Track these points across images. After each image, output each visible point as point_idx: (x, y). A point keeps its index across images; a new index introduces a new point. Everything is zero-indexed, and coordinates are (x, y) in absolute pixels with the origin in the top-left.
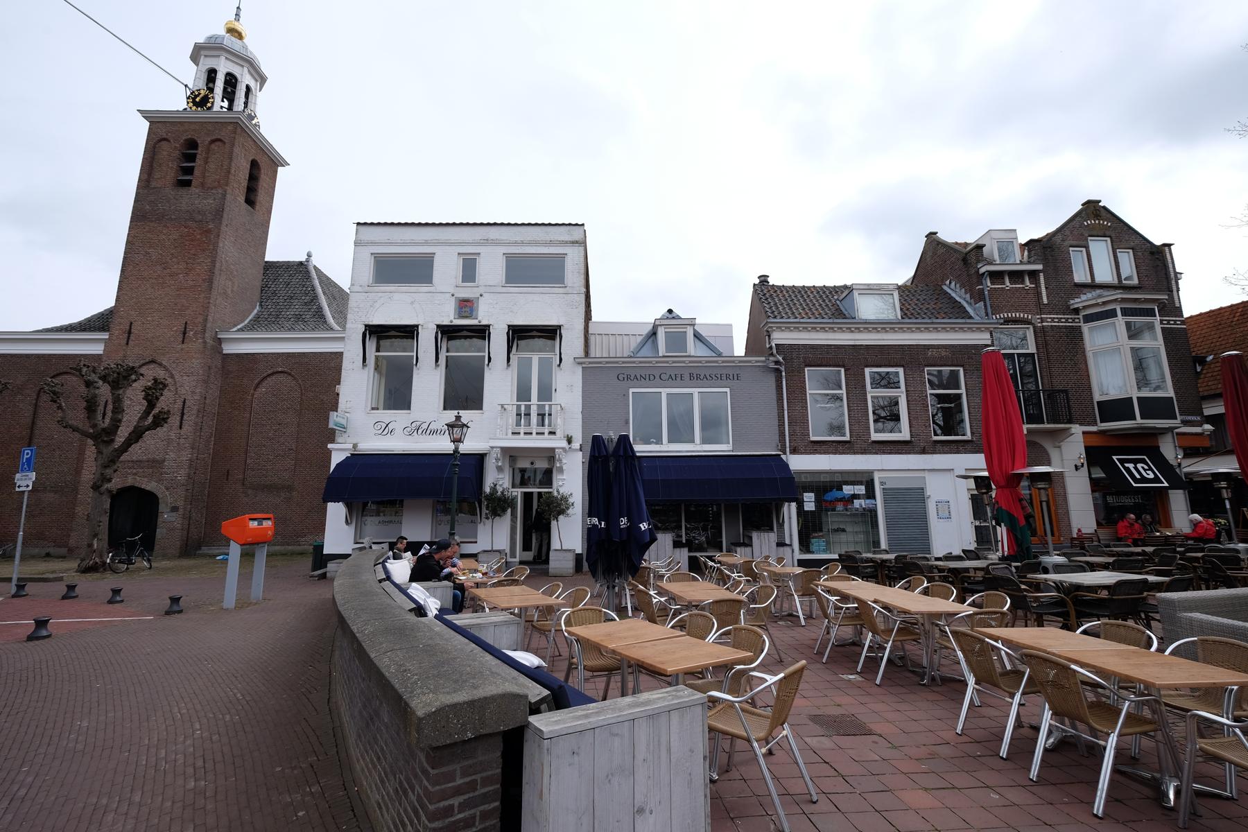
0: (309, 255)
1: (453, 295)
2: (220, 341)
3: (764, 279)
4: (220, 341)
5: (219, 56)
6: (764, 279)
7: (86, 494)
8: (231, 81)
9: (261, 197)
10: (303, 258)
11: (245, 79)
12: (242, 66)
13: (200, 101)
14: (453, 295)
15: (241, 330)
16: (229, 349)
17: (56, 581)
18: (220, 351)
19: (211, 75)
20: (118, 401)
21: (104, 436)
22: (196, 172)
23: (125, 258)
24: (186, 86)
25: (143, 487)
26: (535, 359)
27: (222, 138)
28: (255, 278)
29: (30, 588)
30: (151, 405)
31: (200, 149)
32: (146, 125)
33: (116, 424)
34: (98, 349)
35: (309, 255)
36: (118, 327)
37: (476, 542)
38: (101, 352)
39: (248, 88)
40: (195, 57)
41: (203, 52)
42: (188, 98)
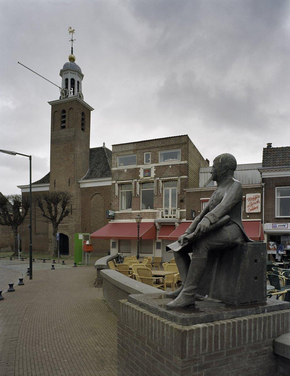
0: (104, 144)
1: (143, 168)
2: (79, 183)
3: (269, 145)
4: (79, 183)
5: (68, 73)
6: (269, 145)
7: (51, 236)
8: (73, 80)
10: (102, 146)
11: (77, 79)
12: (75, 74)
13: (64, 93)
14: (143, 168)
15: (83, 179)
16: (82, 186)
17: (136, 185)
18: (79, 187)
19: (67, 80)
20: (56, 209)
21: (53, 219)
22: (67, 122)
23: (51, 157)
24: (60, 88)
25: (64, 233)
26: (170, 190)
27: (72, 107)
28: (89, 151)
29: (46, 261)
30: (64, 209)
31: (66, 113)
32: (51, 106)
33: (56, 214)
34: (47, 189)
35: (104, 144)
36: (52, 179)
37: (130, 253)
38: (49, 190)
39: (78, 82)
40: (61, 75)
41: (63, 73)
42: (61, 93)
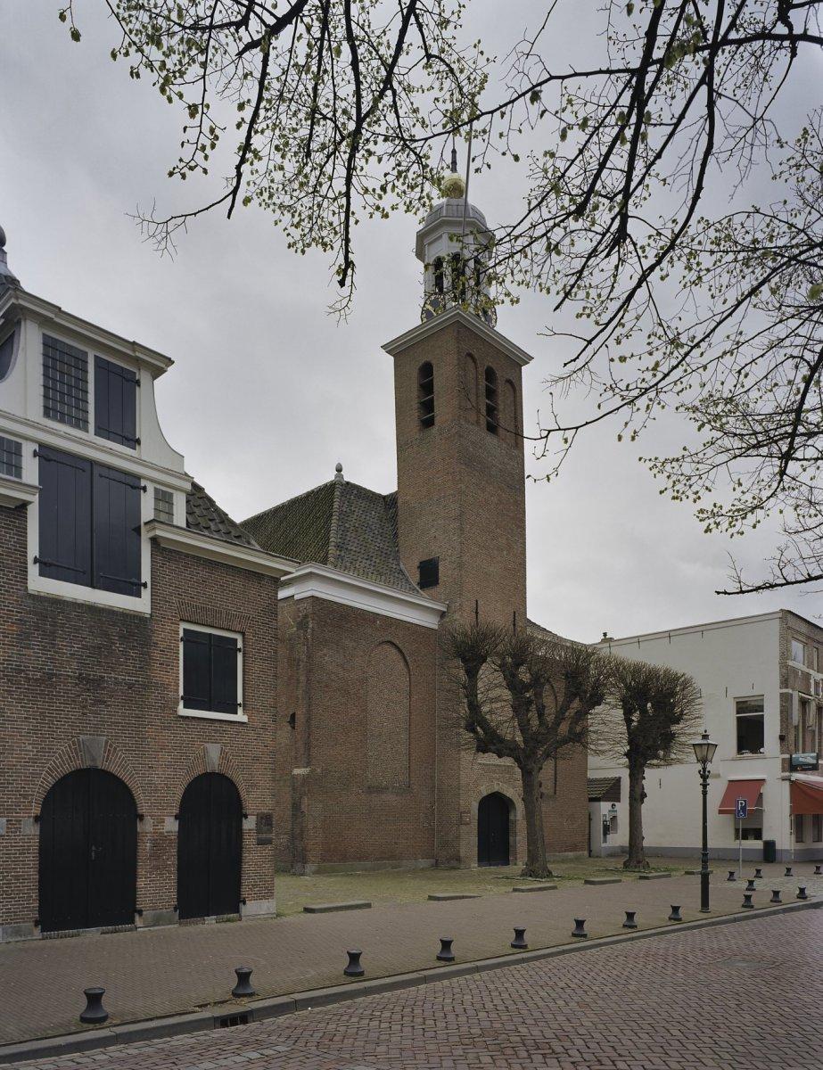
9: (503, 418)
41: (426, 242)
